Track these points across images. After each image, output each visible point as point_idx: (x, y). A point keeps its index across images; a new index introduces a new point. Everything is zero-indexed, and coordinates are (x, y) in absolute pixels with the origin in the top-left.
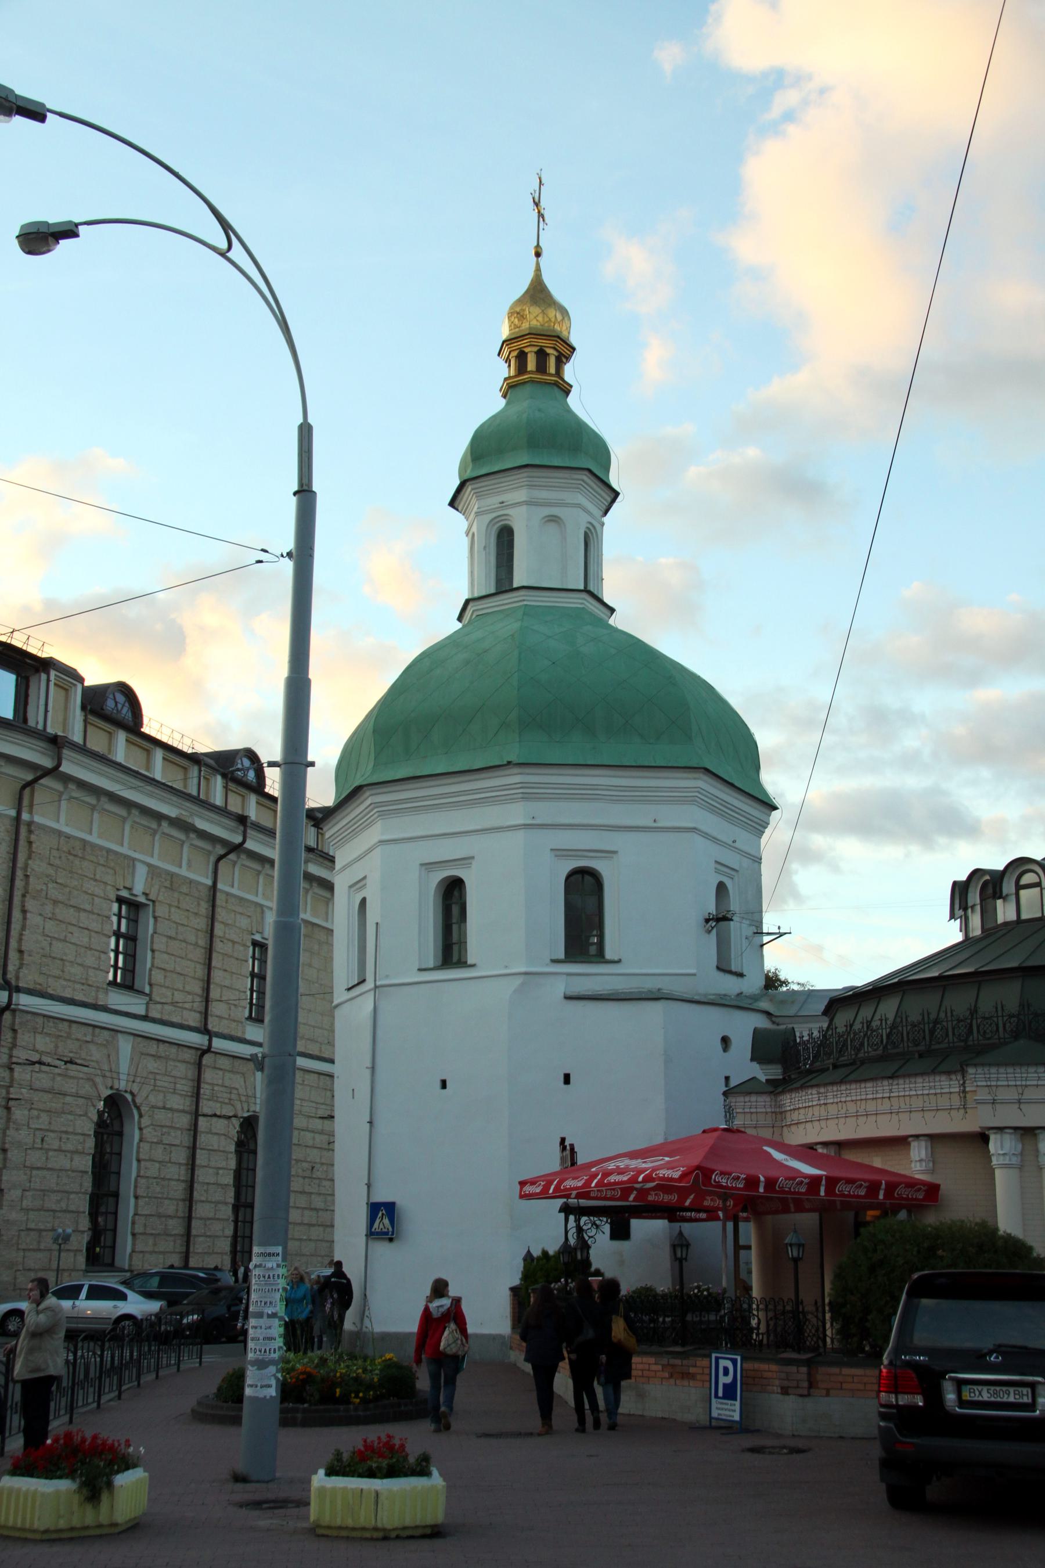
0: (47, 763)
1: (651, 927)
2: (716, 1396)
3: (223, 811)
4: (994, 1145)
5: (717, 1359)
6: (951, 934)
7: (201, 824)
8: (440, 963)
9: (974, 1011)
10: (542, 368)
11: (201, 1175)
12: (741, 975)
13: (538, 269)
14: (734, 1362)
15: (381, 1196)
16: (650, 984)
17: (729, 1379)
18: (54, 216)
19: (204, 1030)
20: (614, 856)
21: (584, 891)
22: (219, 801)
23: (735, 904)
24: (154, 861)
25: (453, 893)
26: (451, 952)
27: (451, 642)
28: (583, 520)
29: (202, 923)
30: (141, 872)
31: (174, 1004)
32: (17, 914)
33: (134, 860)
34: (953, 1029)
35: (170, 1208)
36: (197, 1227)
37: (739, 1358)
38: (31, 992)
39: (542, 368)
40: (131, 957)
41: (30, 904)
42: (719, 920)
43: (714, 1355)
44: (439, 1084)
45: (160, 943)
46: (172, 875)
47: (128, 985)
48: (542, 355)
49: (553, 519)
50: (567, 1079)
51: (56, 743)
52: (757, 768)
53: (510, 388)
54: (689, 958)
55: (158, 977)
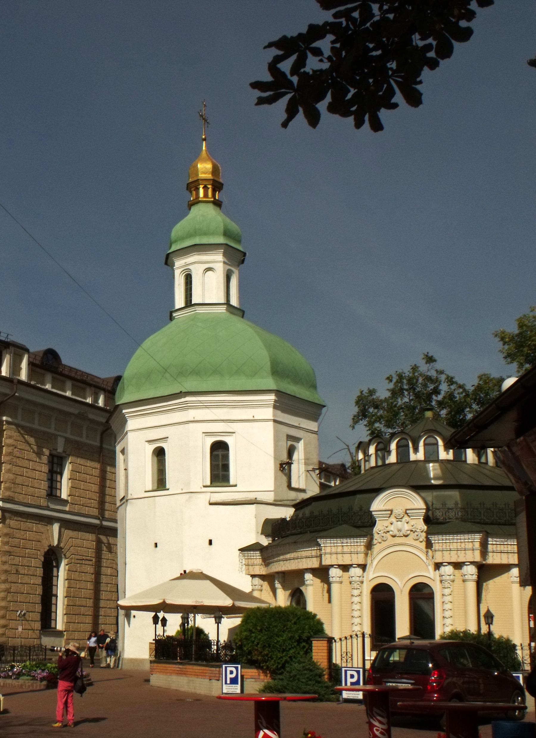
2: (226, 683)
5: (226, 667)
7: (91, 416)
8: (155, 488)
14: (237, 668)
16: (252, 496)
17: (233, 676)
20: (234, 434)
21: (219, 451)
24: (68, 435)
25: (160, 453)
26: (161, 483)
33: (57, 436)
34: (342, 517)
37: (239, 666)
43: (224, 666)
44: (154, 545)
50: (210, 542)
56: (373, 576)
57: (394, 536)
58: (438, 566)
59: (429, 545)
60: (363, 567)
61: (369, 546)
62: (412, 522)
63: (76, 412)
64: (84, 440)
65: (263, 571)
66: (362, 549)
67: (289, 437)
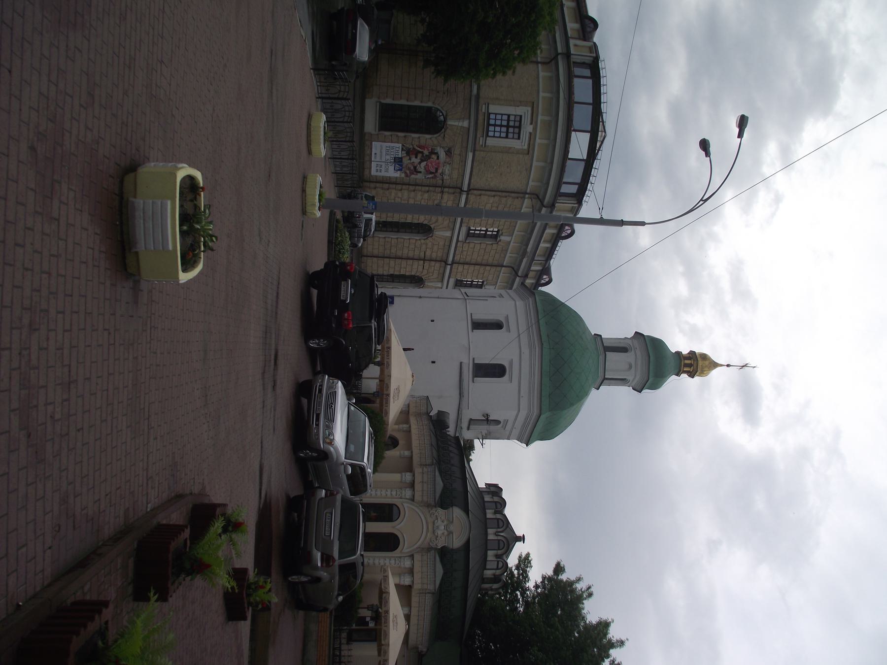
0: (546, 202)
1: (486, 395)
3: (529, 269)
4: (408, 474)
6: (481, 485)
7: (525, 260)
9: (453, 465)
10: (686, 365)
11: (404, 262)
12: (468, 429)
13: (722, 365)
15: (396, 299)
18: (712, 149)
19: (453, 262)
21: (496, 371)
22: (533, 268)
23: (493, 428)
24: (512, 244)
25: (497, 325)
26: (478, 325)
27: (586, 329)
28: (630, 378)
29: (490, 261)
30: (508, 239)
31: (462, 252)
32: (493, 193)
35: (393, 251)
36: (387, 260)
38: (467, 199)
39: (686, 365)
40: (479, 236)
41: (497, 198)
42: (487, 420)
45: (483, 246)
46: (507, 251)
47: (468, 235)
48: (690, 365)
49: (630, 367)
50: (433, 362)
51: (552, 206)
52: (542, 439)
53: (678, 353)
54: (473, 412)
55: (472, 245)
56: (407, 508)
57: (434, 523)
58: (412, 557)
59: (429, 549)
60: (413, 499)
61: (428, 506)
62: (443, 538)
63: (529, 250)
64: (508, 255)
65: (412, 410)
66: (425, 499)
67: (506, 421)
